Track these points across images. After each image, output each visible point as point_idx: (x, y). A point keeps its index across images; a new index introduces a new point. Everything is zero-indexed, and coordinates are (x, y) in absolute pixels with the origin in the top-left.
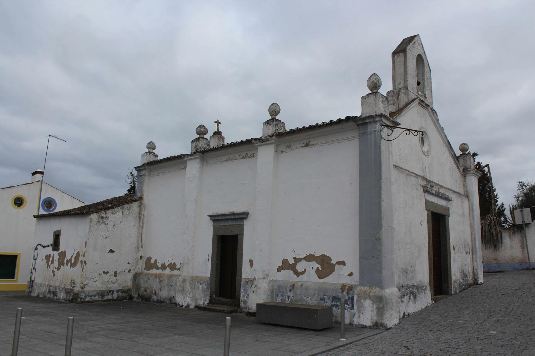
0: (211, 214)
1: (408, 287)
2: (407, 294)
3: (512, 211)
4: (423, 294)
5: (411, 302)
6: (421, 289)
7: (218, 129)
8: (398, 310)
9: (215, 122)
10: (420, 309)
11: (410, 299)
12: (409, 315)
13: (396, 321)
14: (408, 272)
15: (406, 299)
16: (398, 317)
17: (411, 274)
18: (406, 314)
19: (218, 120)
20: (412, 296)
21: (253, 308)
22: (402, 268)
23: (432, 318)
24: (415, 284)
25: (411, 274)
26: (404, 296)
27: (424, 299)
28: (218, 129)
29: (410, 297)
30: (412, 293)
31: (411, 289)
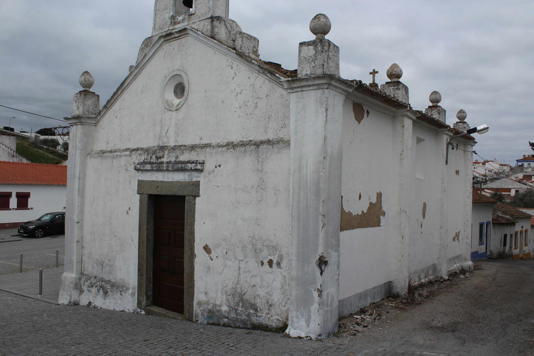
0: (531, 142)
1: (102, 280)
2: (96, 287)
3: (382, 86)
4: (119, 294)
5: (99, 296)
6: (117, 289)
7: (374, 81)
8: (69, 294)
9: (371, 73)
10: (112, 309)
11: (98, 292)
12: (95, 307)
13: (66, 303)
14: (104, 264)
15: (94, 290)
16: (68, 300)
17: (107, 268)
18: (93, 305)
19: (374, 70)
20: (101, 290)
21: (447, 278)
22: (97, 260)
23: (10, 298)
24: (113, 280)
25: (107, 268)
26: (92, 286)
27: (119, 302)
28: (374, 81)
29: (99, 290)
30: (102, 287)
31: (103, 283)
